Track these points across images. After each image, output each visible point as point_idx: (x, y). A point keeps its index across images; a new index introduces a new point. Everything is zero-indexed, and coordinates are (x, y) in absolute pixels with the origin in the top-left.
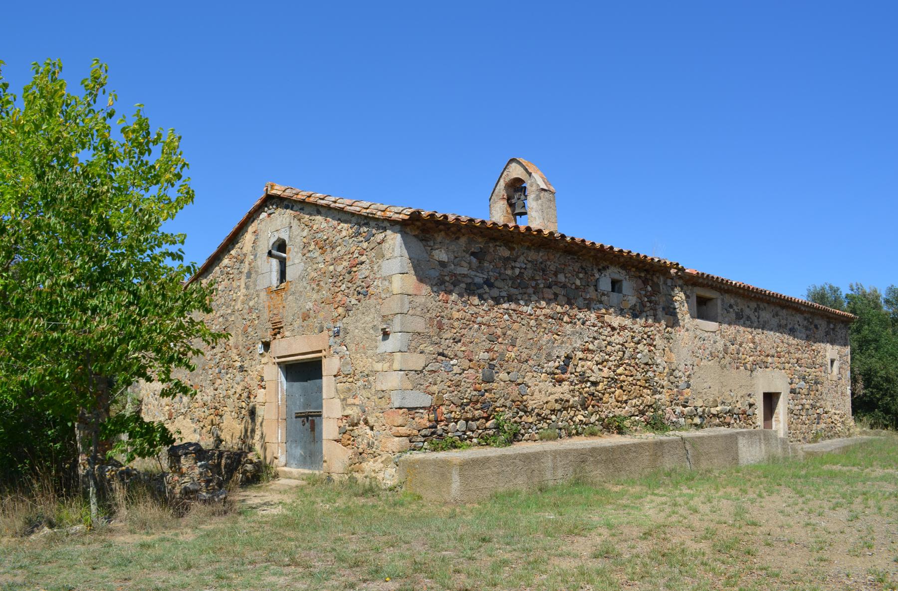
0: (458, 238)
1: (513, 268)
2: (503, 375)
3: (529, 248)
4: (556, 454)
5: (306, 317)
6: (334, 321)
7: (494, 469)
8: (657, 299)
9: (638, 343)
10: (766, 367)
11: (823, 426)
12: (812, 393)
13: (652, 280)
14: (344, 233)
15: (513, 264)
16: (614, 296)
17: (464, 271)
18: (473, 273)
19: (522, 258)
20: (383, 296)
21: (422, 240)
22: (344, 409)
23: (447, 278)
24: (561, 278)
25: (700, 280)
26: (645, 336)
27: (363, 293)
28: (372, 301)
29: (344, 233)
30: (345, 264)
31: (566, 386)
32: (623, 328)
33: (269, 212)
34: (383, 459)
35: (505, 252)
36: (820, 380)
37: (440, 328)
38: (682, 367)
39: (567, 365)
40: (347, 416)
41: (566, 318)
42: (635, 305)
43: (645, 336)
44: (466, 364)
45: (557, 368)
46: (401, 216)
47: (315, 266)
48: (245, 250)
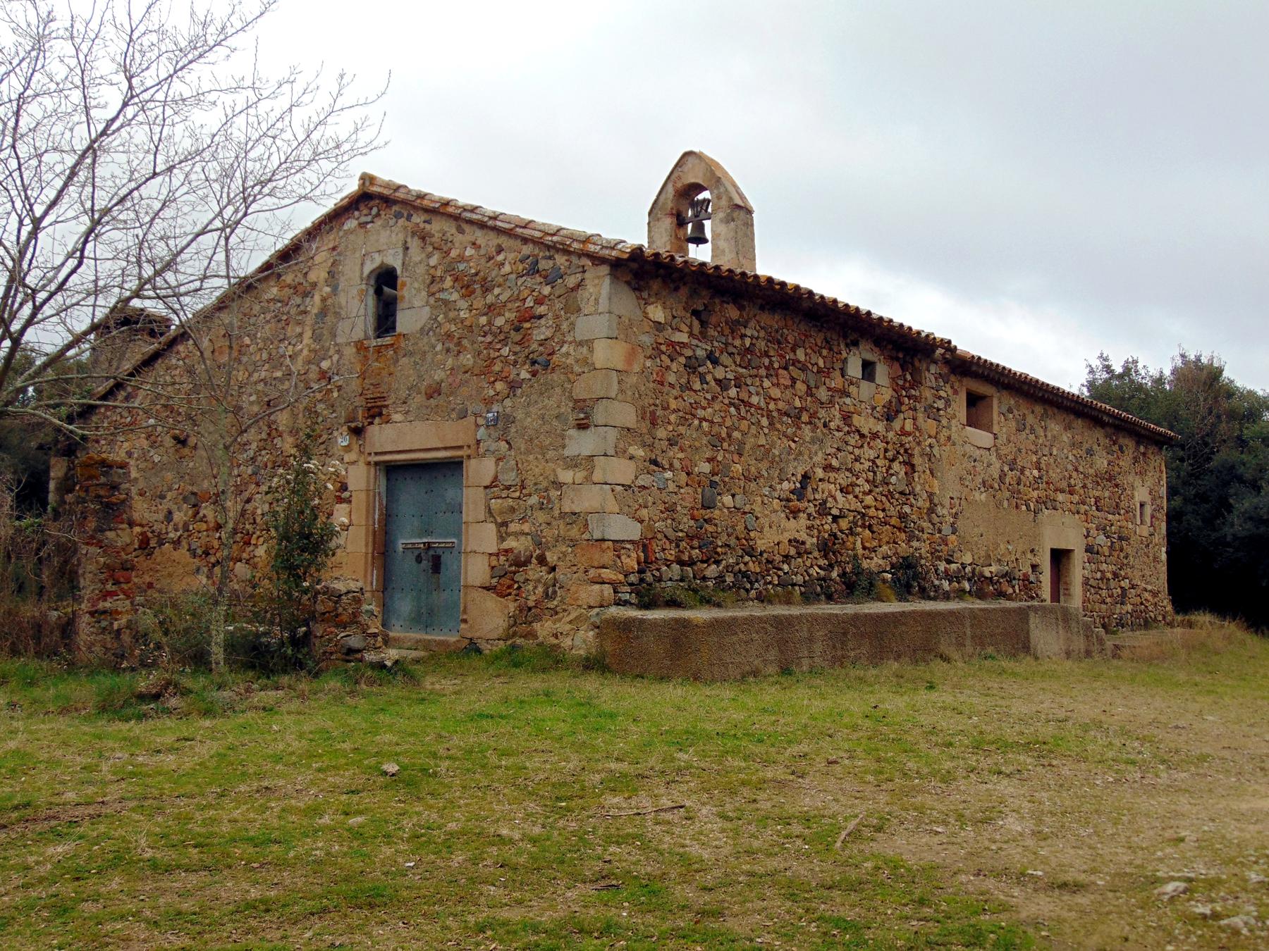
0: (676, 289)
1: (743, 336)
2: (727, 500)
3: (762, 308)
4: (814, 619)
5: (434, 392)
6: (488, 402)
7: (741, 635)
8: (918, 394)
9: (892, 460)
10: (1055, 509)
11: (1129, 608)
12: (1116, 554)
13: (913, 365)
14: (507, 268)
15: (743, 331)
16: (865, 385)
17: (683, 337)
18: (695, 342)
19: (752, 323)
20: (577, 369)
21: (635, 289)
22: (502, 539)
23: (663, 348)
24: (800, 355)
25: (974, 368)
26: (902, 451)
27: (541, 364)
28: (557, 377)
29: (507, 268)
30: (510, 315)
31: (803, 520)
32: (875, 436)
33: (363, 219)
34: (571, 617)
35: (733, 313)
36: (1125, 533)
37: (654, 423)
38: (947, 502)
39: (803, 487)
40: (506, 551)
41: (805, 417)
42: (890, 402)
43: (902, 451)
44: (683, 477)
45: (792, 492)
46: (614, 253)
47: (452, 314)
48: (312, 277)
